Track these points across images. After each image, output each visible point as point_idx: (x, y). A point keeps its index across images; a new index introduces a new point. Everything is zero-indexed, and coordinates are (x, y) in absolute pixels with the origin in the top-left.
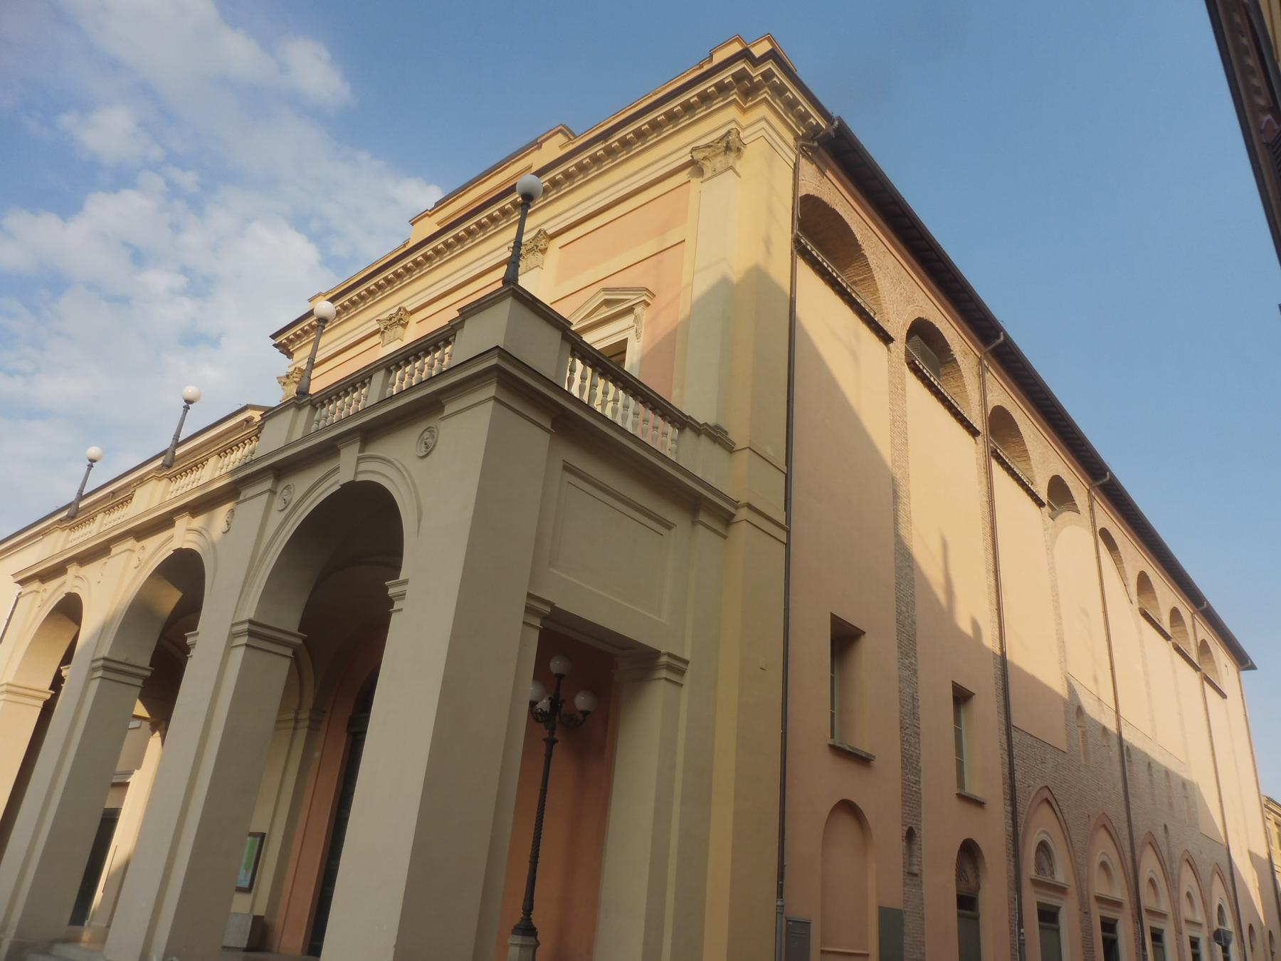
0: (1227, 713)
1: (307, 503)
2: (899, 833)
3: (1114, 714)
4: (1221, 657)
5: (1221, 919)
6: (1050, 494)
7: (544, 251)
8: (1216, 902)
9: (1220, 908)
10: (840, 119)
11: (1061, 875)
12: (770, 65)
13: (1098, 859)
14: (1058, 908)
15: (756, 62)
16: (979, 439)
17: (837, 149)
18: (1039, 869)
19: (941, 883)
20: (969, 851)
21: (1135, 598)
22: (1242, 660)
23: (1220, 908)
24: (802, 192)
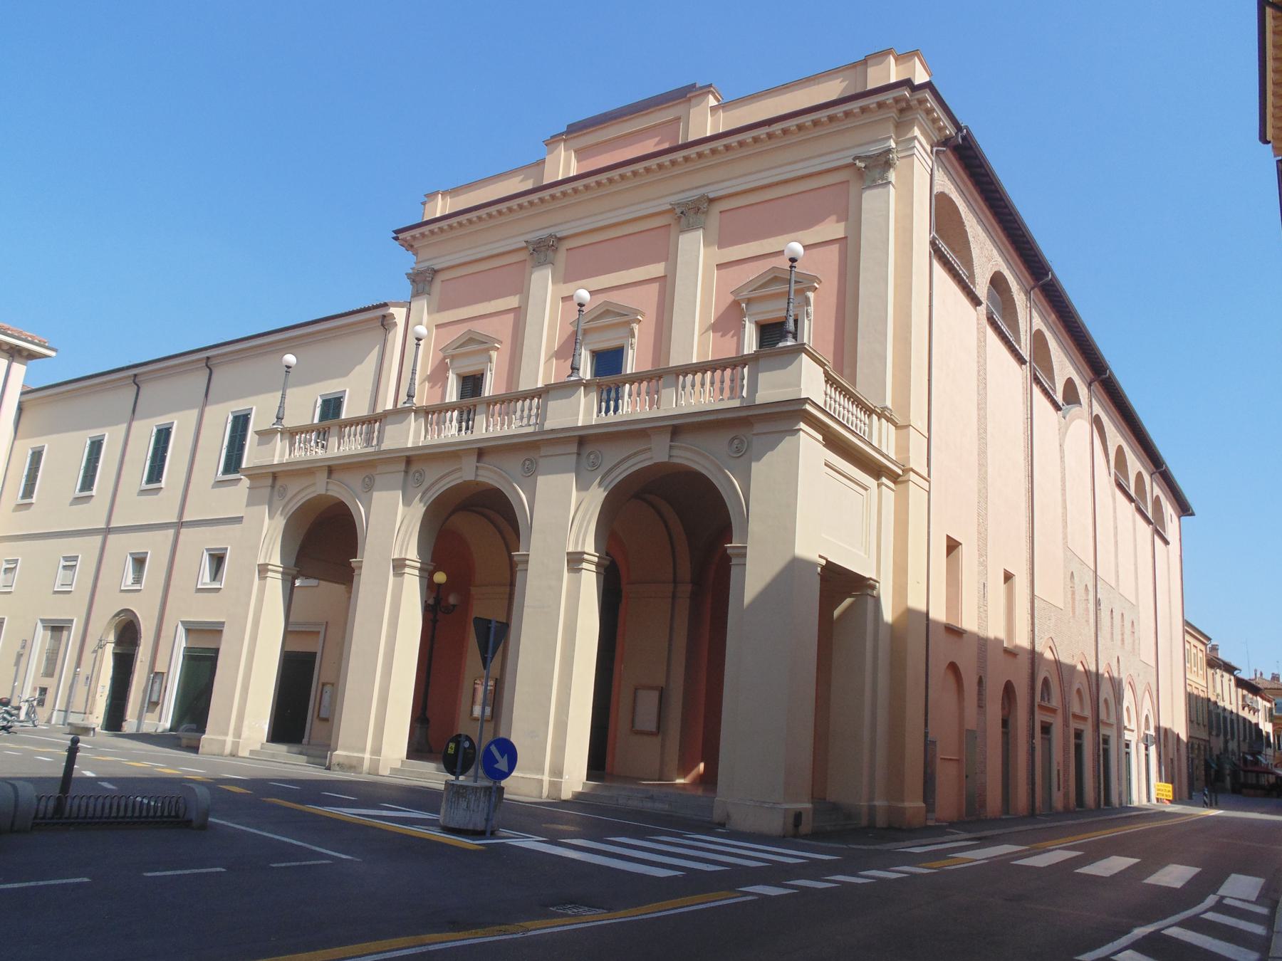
0: (1169, 556)
1: (619, 471)
2: (975, 680)
3: (1091, 573)
4: (1169, 509)
5: (1147, 727)
6: (1064, 399)
7: (706, 213)
8: (1145, 712)
9: (1147, 717)
10: (966, 127)
11: (1055, 702)
12: (927, 95)
13: (1075, 687)
14: (1051, 724)
15: (915, 88)
16: (982, 309)
17: (964, 155)
18: (1043, 698)
19: (994, 710)
20: (1009, 689)
21: (1113, 470)
22: (1184, 509)
23: (1147, 717)
24: (935, 192)
